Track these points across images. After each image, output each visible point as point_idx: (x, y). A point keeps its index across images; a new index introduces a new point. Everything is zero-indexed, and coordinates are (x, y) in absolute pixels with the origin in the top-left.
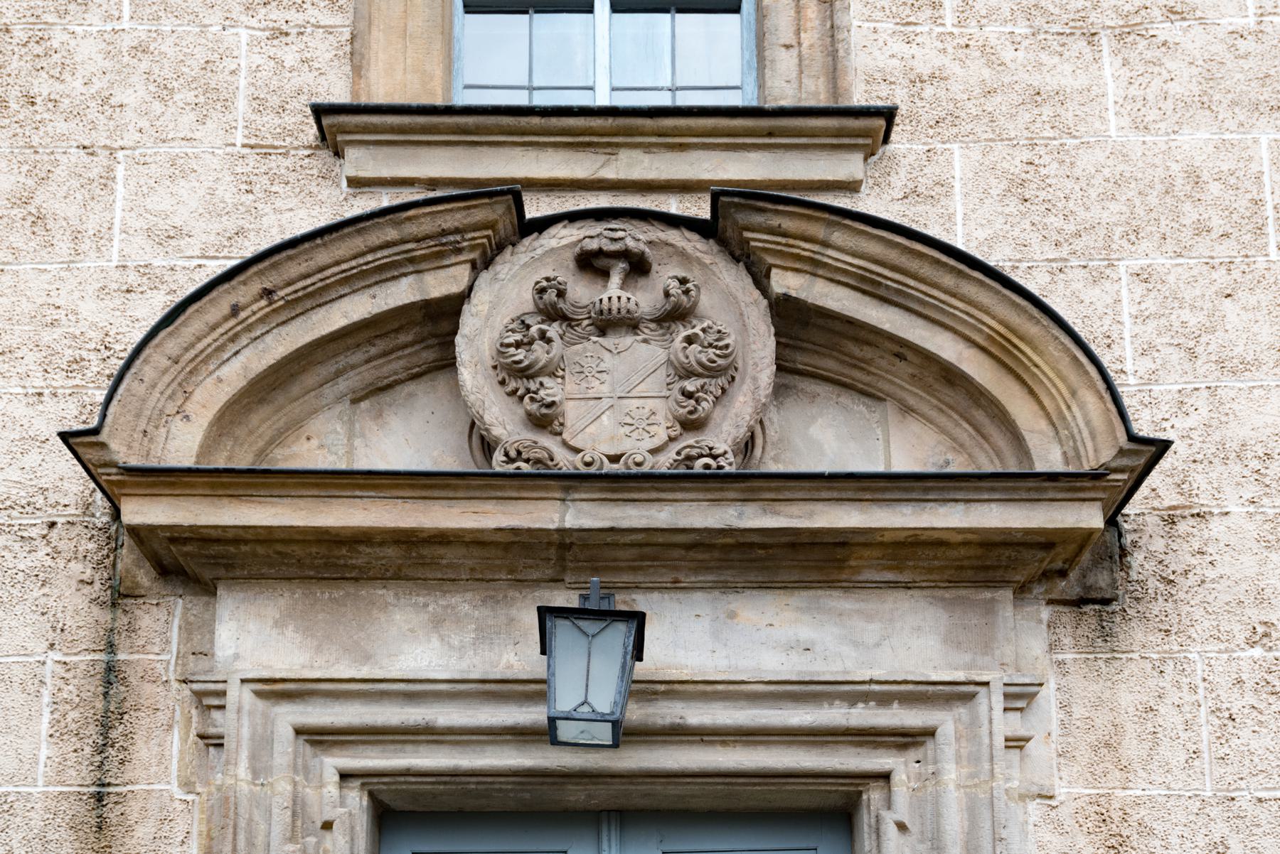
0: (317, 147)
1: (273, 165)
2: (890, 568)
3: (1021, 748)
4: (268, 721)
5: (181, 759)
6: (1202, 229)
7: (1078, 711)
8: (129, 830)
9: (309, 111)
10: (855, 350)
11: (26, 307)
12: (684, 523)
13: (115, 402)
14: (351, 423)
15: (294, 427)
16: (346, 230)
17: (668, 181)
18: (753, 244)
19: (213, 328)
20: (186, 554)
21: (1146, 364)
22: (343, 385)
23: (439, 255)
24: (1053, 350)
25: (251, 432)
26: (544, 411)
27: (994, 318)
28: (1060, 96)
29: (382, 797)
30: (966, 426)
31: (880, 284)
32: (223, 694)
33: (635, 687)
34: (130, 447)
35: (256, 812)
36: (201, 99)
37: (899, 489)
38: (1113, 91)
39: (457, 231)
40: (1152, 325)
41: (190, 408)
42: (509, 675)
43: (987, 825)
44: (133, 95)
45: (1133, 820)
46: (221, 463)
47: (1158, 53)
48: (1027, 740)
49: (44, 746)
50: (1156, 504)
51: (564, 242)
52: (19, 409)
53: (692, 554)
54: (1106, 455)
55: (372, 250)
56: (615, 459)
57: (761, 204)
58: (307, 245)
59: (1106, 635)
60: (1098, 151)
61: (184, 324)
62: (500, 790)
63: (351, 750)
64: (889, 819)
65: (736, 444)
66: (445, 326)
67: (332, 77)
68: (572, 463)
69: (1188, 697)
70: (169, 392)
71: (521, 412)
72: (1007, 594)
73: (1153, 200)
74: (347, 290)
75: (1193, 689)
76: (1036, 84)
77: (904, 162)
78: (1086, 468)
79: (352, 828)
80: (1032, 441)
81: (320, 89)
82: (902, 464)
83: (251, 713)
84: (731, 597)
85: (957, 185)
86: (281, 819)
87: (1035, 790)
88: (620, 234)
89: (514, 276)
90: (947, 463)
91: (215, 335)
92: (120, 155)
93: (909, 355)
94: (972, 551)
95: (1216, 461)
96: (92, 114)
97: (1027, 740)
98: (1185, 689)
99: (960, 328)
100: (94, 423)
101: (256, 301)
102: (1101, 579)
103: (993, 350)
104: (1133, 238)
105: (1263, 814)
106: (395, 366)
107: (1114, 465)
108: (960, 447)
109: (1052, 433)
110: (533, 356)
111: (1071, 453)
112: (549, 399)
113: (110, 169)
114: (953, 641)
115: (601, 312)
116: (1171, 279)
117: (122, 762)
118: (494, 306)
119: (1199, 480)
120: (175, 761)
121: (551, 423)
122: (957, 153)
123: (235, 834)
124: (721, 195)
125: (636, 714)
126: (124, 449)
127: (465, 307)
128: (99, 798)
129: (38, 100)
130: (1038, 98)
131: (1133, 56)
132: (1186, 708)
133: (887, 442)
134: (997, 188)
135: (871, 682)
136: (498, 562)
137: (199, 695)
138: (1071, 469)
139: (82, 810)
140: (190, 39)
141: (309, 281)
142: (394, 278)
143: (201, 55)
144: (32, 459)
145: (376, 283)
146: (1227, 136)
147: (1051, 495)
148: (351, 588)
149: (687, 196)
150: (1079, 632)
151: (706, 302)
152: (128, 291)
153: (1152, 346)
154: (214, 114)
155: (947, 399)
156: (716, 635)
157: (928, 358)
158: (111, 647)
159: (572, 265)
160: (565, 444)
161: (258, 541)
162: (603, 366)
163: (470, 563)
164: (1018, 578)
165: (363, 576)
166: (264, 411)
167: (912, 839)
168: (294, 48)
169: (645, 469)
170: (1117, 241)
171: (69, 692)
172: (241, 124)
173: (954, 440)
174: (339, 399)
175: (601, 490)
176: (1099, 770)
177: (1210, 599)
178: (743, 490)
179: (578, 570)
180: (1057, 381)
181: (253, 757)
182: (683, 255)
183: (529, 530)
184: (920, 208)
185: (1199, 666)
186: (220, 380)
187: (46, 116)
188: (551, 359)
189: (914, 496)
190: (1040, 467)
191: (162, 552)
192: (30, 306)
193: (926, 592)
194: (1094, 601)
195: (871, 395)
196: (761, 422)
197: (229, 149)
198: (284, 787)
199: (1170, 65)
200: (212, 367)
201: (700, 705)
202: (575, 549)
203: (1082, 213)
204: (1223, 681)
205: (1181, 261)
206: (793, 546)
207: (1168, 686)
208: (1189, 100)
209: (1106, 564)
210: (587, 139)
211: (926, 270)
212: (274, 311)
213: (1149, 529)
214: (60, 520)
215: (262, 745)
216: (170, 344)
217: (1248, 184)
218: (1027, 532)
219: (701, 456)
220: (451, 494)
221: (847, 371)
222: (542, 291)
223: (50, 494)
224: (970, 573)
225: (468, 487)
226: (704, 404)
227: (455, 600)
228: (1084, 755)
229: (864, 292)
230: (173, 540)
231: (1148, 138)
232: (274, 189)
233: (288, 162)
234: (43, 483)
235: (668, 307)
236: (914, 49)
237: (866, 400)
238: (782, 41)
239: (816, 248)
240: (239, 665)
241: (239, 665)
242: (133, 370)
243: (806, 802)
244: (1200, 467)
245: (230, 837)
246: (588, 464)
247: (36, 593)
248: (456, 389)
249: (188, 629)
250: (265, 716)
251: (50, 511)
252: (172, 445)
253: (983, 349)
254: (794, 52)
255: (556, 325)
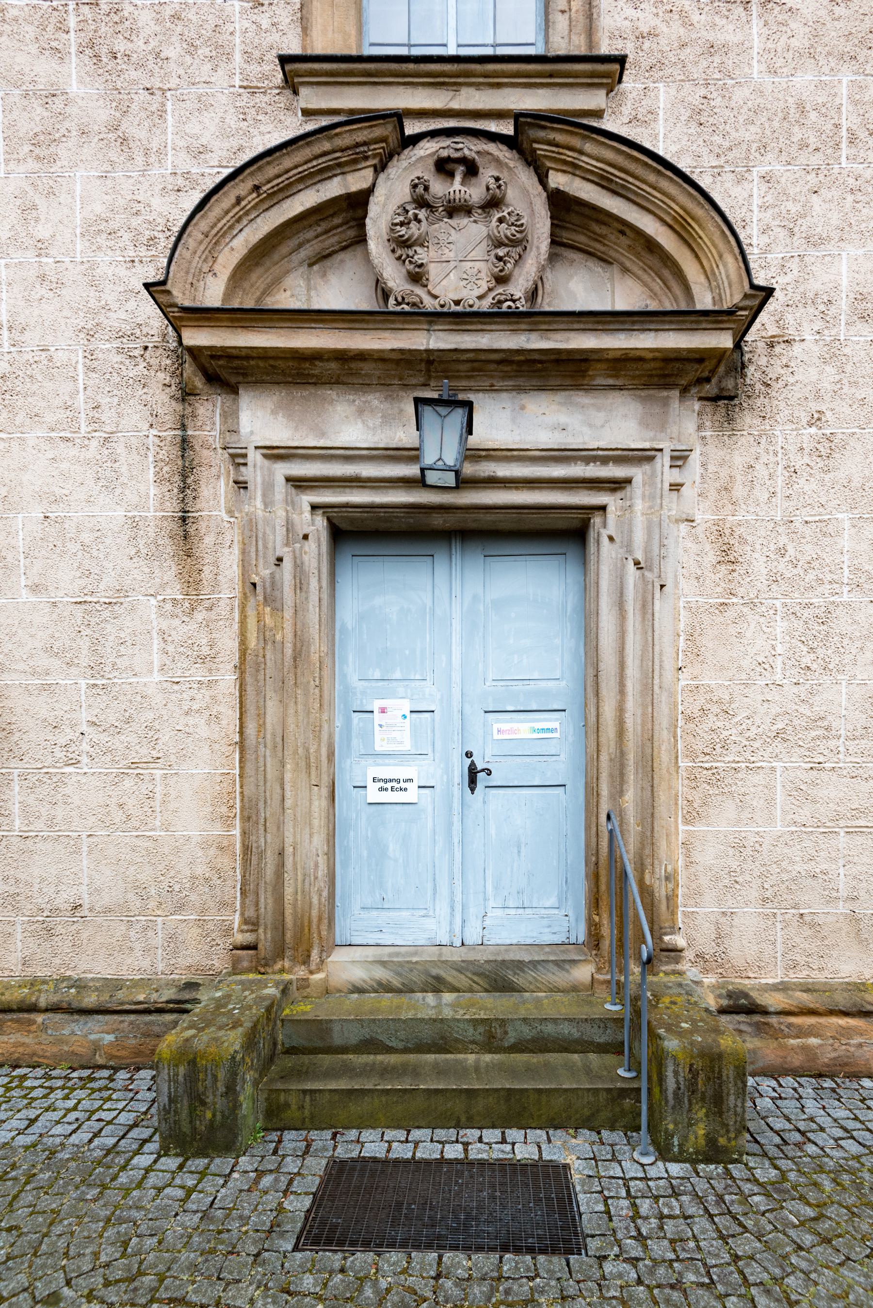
0: (283, 88)
1: (258, 100)
2: (611, 376)
3: (678, 490)
4: (271, 473)
5: (226, 497)
6: (803, 145)
7: (711, 468)
8: (201, 539)
9: (277, 61)
10: (596, 228)
11: (121, 202)
12: (496, 345)
13: (173, 263)
14: (309, 280)
15: (275, 283)
16: (301, 143)
17: (490, 110)
18: (539, 152)
19: (227, 212)
20: (220, 366)
21: (765, 240)
22: (303, 253)
23: (355, 161)
24: (711, 227)
25: (252, 286)
26: (417, 270)
27: (677, 204)
28: (725, 48)
29: (335, 521)
30: (659, 281)
31: (612, 181)
32: (245, 456)
33: (469, 453)
34: (184, 294)
35: (267, 528)
36: (214, 53)
37: (618, 322)
38: (757, 44)
39: (365, 144)
40: (770, 212)
41: (217, 268)
42: (400, 445)
43: (657, 537)
44: (172, 52)
45: (736, 535)
46: (236, 305)
47: (786, 17)
48: (682, 485)
49: (152, 487)
50: (764, 334)
51: (428, 152)
52: (122, 271)
53: (501, 367)
54: (737, 298)
55: (316, 157)
56: (457, 303)
57: (543, 123)
58: (278, 154)
59: (730, 420)
60: (745, 88)
61: (210, 209)
62: (397, 517)
63: (317, 492)
64: (604, 533)
65: (527, 293)
66: (360, 212)
67: (290, 36)
68: (433, 305)
69: (773, 459)
70: (204, 257)
71: (404, 271)
72: (676, 393)
73: (776, 124)
74: (302, 187)
75: (776, 454)
76: (711, 39)
77: (630, 96)
78: (725, 308)
79: (319, 539)
80: (696, 289)
81: (284, 46)
82: (620, 306)
83: (262, 468)
84: (523, 396)
85: (661, 113)
86: (281, 532)
87: (684, 516)
88: (460, 146)
89: (399, 177)
90: (647, 306)
91: (228, 218)
92: (168, 94)
93: (628, 231)
94: (658, 364)
95: (800, 305)
96: (151, 65)
97: (682, 485)
98: (771, 453)
99: (657, 212)
100: (160, 277)
101: (250, 194)
102: (729, 384)
103: (676, 227)
104: (762, 151)
105: (807, 531)
106: (331, 241)
107: (741, 305)
108: (654, 295)
109: (707, 285)
110: (410, 232)
111: (717, 298)
112: (420, 262)
113: (163, 105)
114: (644, 424)
115: (449, 201)
116: (783, 180)
117: (194, 498)
118: (387, 198)
119: (789, 318)
120: (223, 498)
121: (421, 278)
122: (662, 90)
123: (257, 541)
124: (518, 117)
125: (469, 469)
126: (180, 295)
127: (371, 198)
128: (184, 519)
129: (119, 55)
130: (712, 50)
131: (771, 19)
132: (771, 466)
133: (613, 292)
134: (685, 114)
135: (598, 449)
136: (393, 373)
137: (233, 456)
138: (716, 308)
139: (175, 526)
140: (205, 9)
141: (280, 180)
142: (330, 178)
143: (212, 21)
144: (131, 305)
145: (319, 181)
146: (823, 78)
147: (704, 326)
148: (312, 389)
149: (501, 122)
150: (715, 418)
151: (511, 194)
152: (178, 191)
153: (769, 227)
154: (222, 64)
155: (648, 262)
156: (514, 420)
157: (639, 233)
158: (184, 427)
159: (433, 168)
160: (429, 293)
161: (259, 358)
162: (451, 239)
163: (377, 373)
164: (683, 382)
165: (318, 382)
166: (259, 270)
167: (616, 546)
168: (267, 15)
169: (475, 309)
170: (754, 154)
171: (163, 454)
172: (238, 71)
173: (651, 290)
174: (301, 264)
175: (450, 323)
176: (720, 504)
177: (789, 396)
178: (529, 323)
179: (438, 378)
180: (712, 248)
181: (264, 495)
182: (497, 161)
183: (410, 351)
184: (639, 130)
185: (780, 439)
186: (232, 249)
187: (124, 66)
188: (421, 235)
189: (626, 327)
190: (699, 307)
191: (207, 365)
192: (124, 201)
193: (632, 392)
194: (725, 398)
195: (605, 261)
196: (541, 278)
197: (232, 89)
198: (281, 513)
199: (793, 25)
200: (227, 240)
201: (504, 464)
202: (436, 364)
203: (734, 134)
204: (792, 448)
205: (789, 167)
206: (558, 361)
207: (762, 452)
208: (801, 51)
209: (733, 374)
210: (441, 80)
211: (639, 171)
212: (261, 201)
213: (759, 351)
214: (150, 345)
215: (268, 487)
216: (203, 224)
217: (833, 113)
218: (689, 350)
219: (507, 300)
220: (365, 326)
221: (592, 243)
222: (415, 186)
223: (143, 328)
224: (656, 379)
225: (375, 321)
226: (509, 265)
227: (370, 397)
228: (712, 495)
229: (603, 187)
230: (212, 357)
231: (776, 80)
232: (259, 118)
233: (266, 99)
234: (139, 320)
235: (488, 198)
236: (639, 14)
237: (602, 264)
238: (560, 8)
239: (575, 155)
240: (253, 438)
241: (253, 438)
242: (182, 242)
243: (561, 525)
244: (790, 309)
245: (254, 543)
246: (442, 306)
247: (141, 392)
248: (367, 254)
249: (225, 415)
250: (269, 470)
251: (144, 339)
252: (208, 293)
253: (671, 227)
254: (567, 15)
255: (423, 210)
